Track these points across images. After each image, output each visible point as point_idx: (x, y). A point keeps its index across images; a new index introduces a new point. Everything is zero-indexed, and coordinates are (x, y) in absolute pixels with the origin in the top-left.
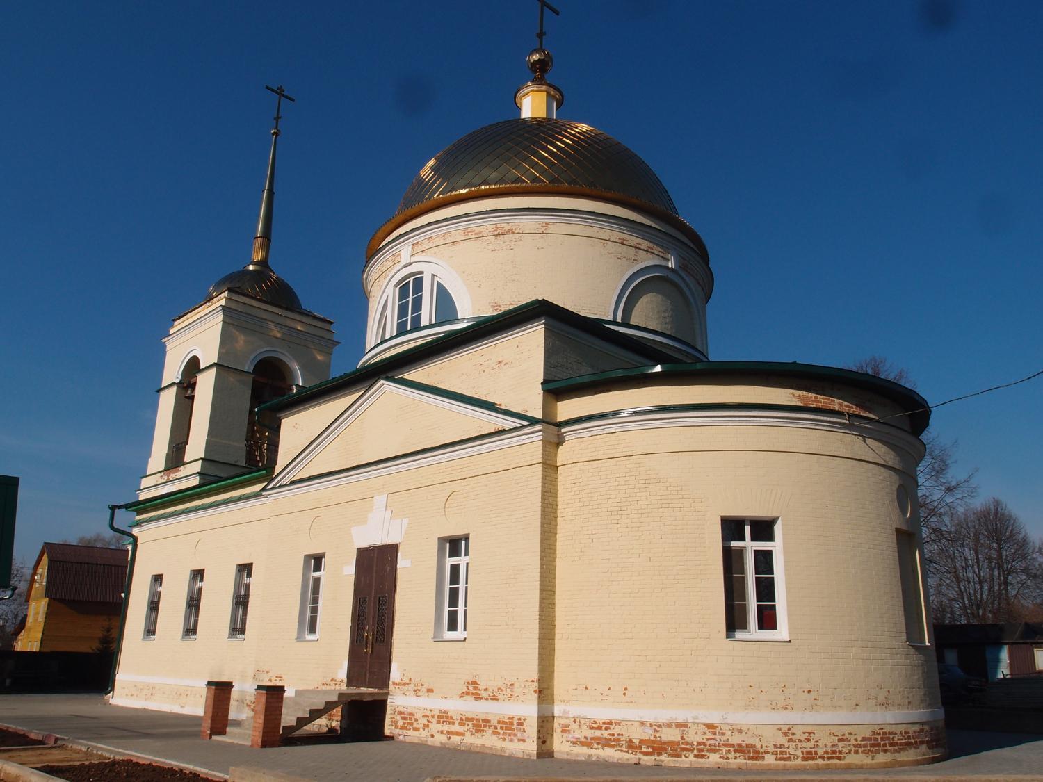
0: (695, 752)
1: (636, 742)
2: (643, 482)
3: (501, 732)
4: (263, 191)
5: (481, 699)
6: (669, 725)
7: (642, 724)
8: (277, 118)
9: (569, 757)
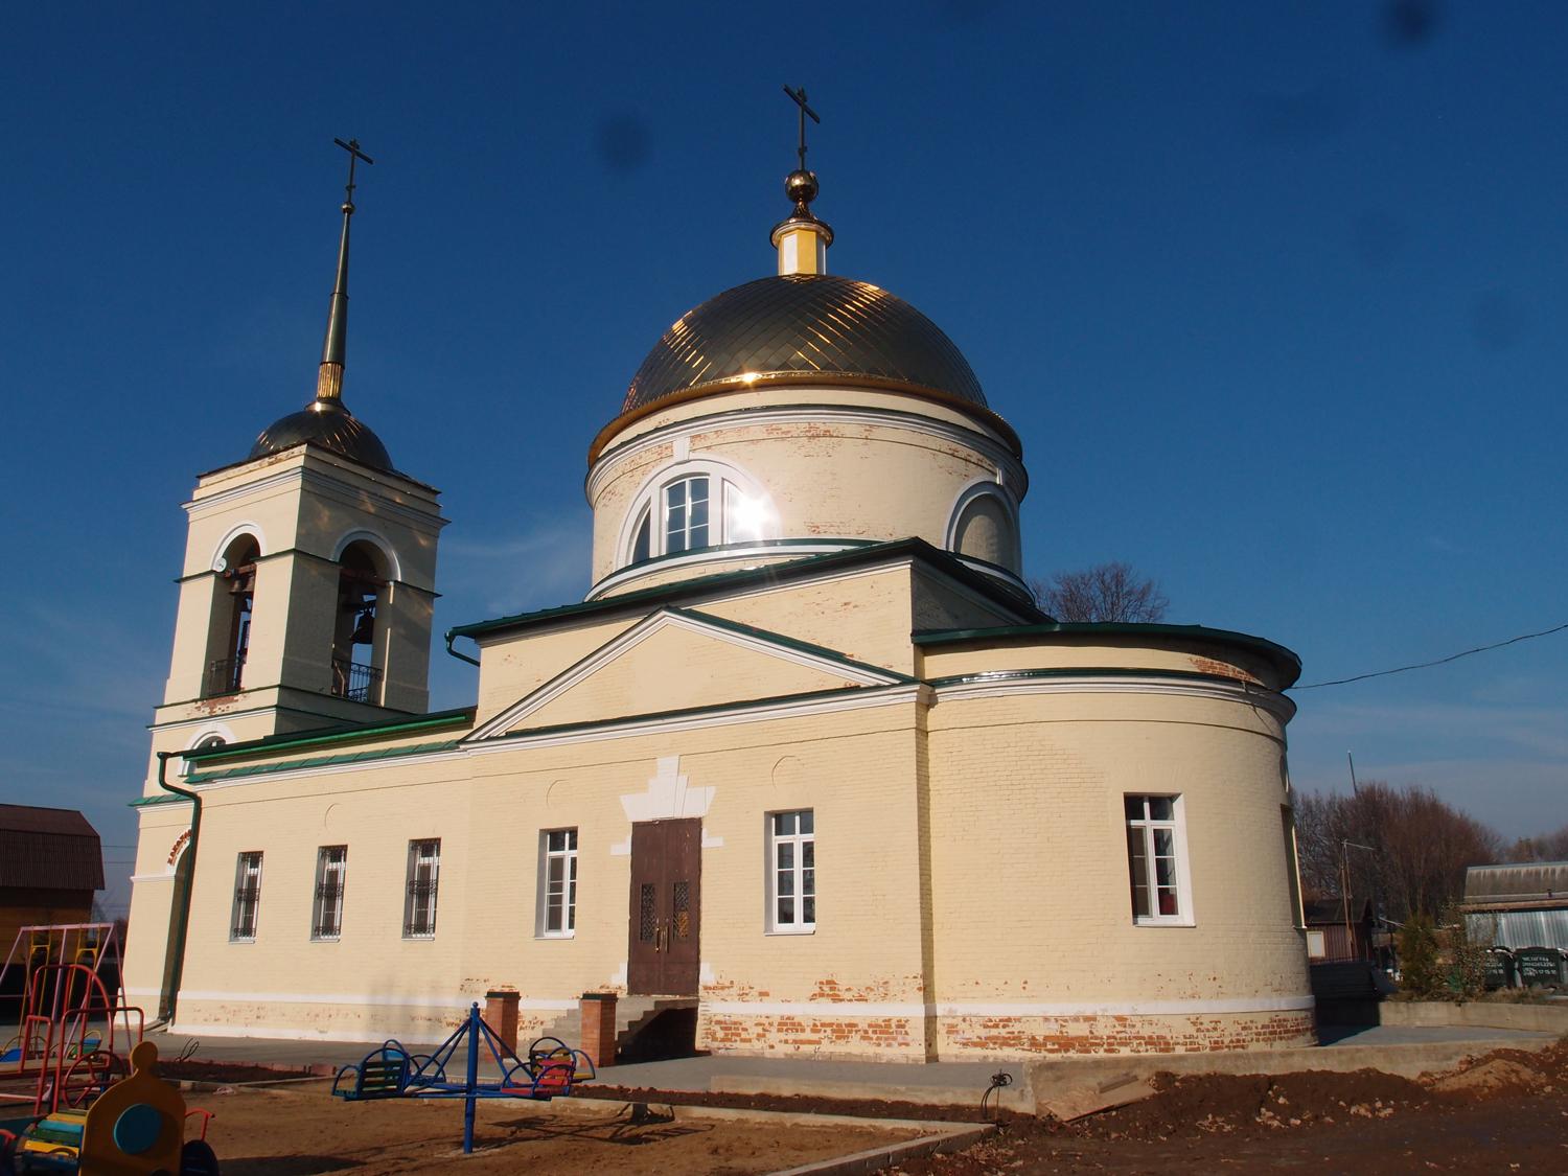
0: (1105, 1046)
1: (1040, 1039)
2: (1037, 753)
3: (875, 1036)
4: (332, 295)
5: (841, 1000)
6: (1076, 1019)
7: (1046, 1019)
8: (350, 188)
9: (958, 1060)
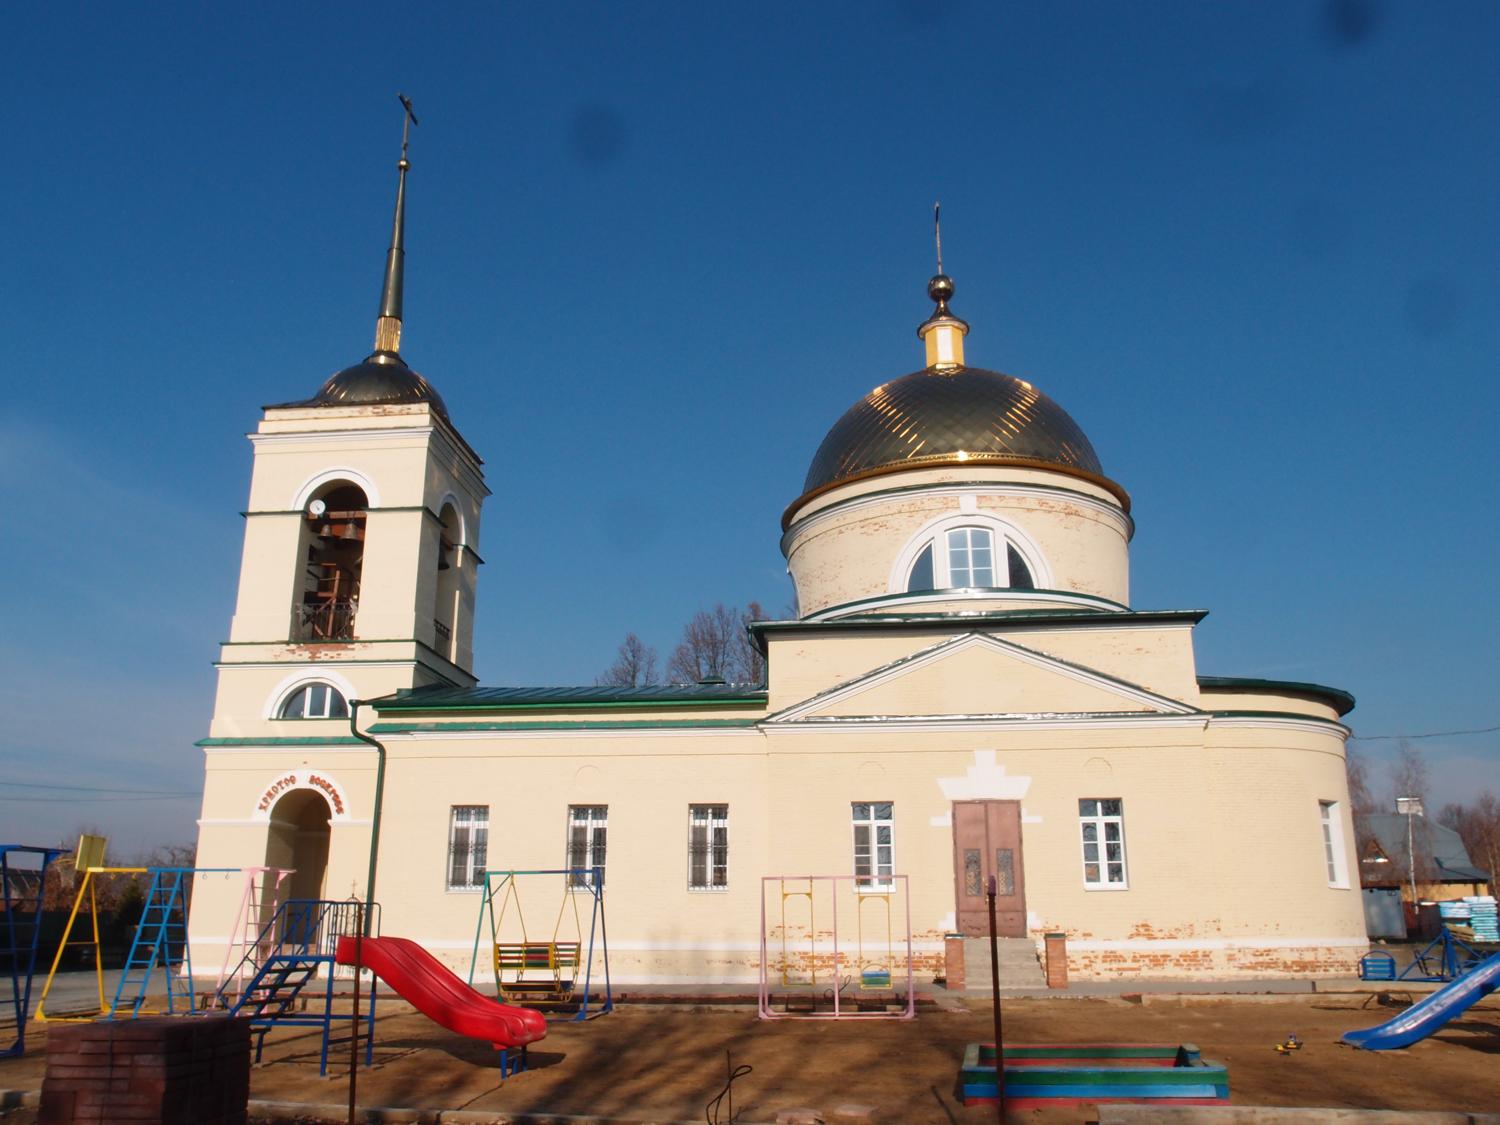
1: (1289, 963)
3: (1185, 963)
5: (1155, 938)
6: (1307, 949)
7: (1292, 950)
